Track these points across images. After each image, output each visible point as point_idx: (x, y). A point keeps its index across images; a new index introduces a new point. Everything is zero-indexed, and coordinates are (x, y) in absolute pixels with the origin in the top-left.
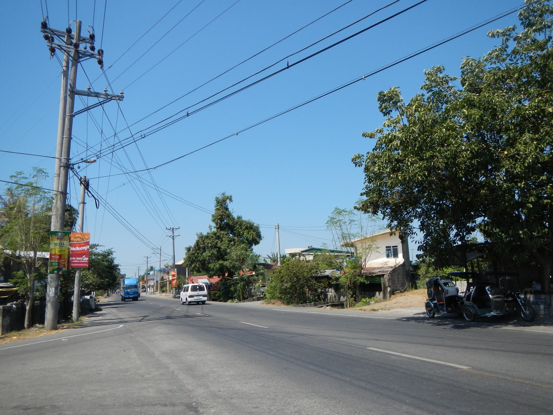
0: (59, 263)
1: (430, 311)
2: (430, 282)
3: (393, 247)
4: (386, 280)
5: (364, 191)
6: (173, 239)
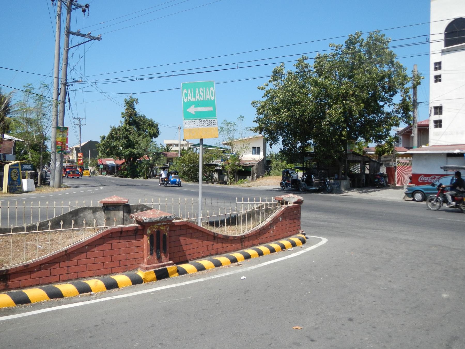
0: (61, 147)
1: (282, 187)
2: (284, 171)
3: (257, 147)
4: (255, 169)
5: (255, 120)
6: (80, 127)
